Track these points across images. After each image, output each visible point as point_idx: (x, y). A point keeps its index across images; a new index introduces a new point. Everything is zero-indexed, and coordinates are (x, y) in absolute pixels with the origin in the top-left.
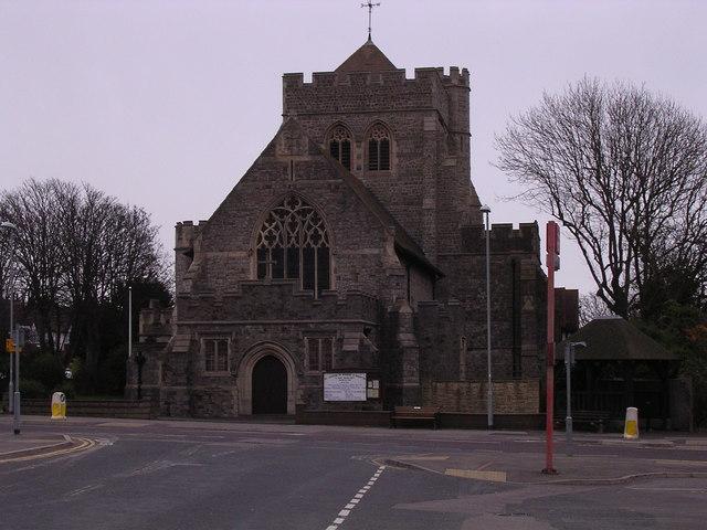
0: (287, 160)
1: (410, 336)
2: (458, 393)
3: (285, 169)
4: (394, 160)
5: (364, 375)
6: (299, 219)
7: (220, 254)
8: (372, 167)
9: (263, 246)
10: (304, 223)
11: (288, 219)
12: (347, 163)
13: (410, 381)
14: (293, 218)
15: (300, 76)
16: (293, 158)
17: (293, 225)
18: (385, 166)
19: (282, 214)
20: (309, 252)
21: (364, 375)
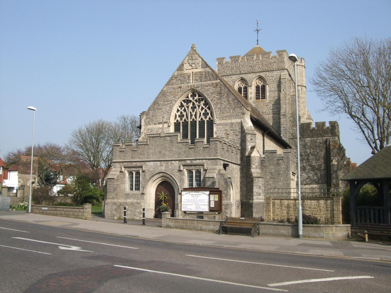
0: (191, 71)
1: (259, 171)
2: (288, 207)
3: (189, 77)
4: (268, 94)
5: (208, 193)
6: (196, 104)
7: (154, 126)
8: (257, 98)
9: (177, 121)
10: (199, 106)
11: (191, 105)
12: (246, 96)
13: (257, 199)
14: (194, 104)
15: (324, 124)
16: (192, 70)
17: (194, 108)
18: (264, 97)
19: (188, 101)
20: (202, 123)
21: (208, 193)
